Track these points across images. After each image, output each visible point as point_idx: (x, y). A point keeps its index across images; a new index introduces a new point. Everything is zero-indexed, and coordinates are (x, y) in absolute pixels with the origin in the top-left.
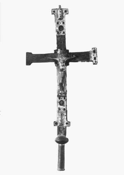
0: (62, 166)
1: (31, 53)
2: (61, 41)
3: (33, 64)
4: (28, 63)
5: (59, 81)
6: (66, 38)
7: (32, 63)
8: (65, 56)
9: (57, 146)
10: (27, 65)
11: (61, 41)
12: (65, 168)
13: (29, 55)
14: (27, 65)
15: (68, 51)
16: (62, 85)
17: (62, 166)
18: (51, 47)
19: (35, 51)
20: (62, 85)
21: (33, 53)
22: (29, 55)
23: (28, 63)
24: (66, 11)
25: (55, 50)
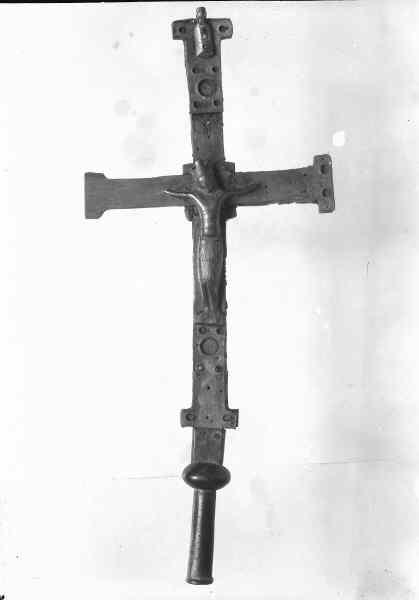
0: (203, 571)
1: (101, 176)
2: (213, 246)
3: (111, 215)
4: (94, 210)
5: (201, 272)
6: (225, 121)
7: (108, 209)
8: (216, 190)
9: (186, 497)
10: (88, 217)
11: (213, 246)
12: (213, 575)
13: (94, 181)
14: (88, 217)
15: (232, 165)
16: (212, 297)
17: (203, 571)
18: (175, 155)
19: (118, 169)
20: (212, 297)
21: (110, 175)
22: (94, 181)
23: (94, 210)
24: (222, 28)
25: (233, 165)
